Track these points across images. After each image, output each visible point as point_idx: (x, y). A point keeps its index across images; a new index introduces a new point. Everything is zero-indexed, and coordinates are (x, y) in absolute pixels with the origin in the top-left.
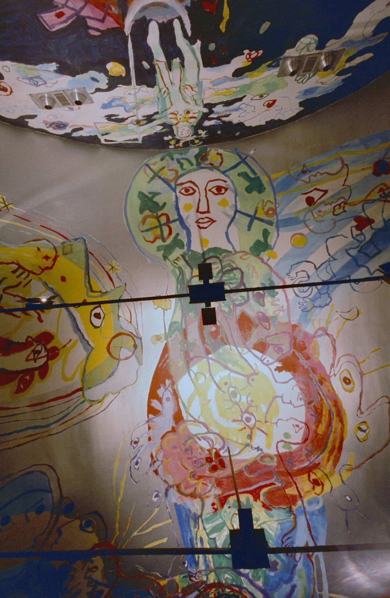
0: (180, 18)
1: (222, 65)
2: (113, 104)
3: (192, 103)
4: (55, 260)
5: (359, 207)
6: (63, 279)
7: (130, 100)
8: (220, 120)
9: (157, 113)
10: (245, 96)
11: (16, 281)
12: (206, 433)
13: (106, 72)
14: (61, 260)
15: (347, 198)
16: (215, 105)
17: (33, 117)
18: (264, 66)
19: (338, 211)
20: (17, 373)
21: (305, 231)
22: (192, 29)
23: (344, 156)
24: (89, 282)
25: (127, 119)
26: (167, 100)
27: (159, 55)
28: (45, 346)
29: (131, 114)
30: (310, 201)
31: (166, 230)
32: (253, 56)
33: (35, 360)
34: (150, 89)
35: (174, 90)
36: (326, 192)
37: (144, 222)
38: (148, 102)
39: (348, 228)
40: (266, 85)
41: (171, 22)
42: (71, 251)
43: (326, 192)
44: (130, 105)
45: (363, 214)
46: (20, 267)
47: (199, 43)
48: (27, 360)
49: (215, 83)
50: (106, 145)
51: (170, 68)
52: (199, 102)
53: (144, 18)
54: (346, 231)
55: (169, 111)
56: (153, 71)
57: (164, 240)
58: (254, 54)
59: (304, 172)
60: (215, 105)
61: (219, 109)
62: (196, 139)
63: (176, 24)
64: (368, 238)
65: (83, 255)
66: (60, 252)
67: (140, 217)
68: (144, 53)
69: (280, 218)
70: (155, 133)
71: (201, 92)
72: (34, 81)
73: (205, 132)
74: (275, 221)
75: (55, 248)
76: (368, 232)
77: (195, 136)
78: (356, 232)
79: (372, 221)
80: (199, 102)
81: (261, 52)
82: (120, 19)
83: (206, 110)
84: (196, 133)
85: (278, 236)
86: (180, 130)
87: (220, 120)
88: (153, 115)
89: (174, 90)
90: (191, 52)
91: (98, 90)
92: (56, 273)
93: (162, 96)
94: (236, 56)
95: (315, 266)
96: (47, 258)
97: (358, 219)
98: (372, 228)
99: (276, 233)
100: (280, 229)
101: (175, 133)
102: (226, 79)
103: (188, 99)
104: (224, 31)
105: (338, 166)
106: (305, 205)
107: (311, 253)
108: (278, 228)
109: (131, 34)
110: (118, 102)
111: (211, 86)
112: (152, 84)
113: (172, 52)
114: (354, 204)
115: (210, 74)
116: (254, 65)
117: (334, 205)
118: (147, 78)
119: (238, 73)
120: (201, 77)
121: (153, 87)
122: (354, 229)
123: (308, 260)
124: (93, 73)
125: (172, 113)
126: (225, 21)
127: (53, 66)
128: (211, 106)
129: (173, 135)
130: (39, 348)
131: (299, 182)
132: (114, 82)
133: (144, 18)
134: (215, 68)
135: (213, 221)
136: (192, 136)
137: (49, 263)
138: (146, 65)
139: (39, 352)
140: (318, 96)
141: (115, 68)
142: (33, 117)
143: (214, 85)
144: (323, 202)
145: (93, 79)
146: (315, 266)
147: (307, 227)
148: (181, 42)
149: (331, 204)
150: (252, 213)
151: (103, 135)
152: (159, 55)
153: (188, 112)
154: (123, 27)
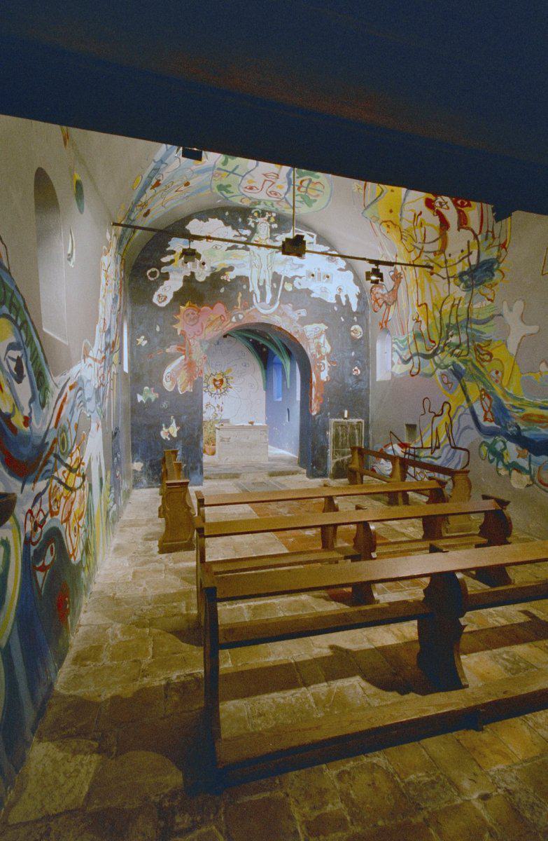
1: (300, 444)
4: (386, 222)
5: (158, 191)
6: (391, 211)
11: (409, 238)
13: (293, 286)
14: (383, 218)
17: (341, 270)
19: (170, 184)
20: (459, 212)
24: (380, 196)
27: (268, 288)
28: (434, 201)
30: (187, 184)
31: (305, 184)
33: (446, 203)
35: (264, 267)
36: (176, 191)
37: (318, 196)
42: (374, 216)
43: (176, 191)
46: (402, 238)
48: (448, 208)
49: (242, 265)
50: (315, 232)
51: (265, 281)
56: (273, 281)
57: (310, 181)
60: (243, 248)
63: (259, 301)
65: (369, 210)
66: (379, 222)
67: (318, 199)
68: (274, 291)
72: (325, 291)
75: (380, 225)
77: (257, 221)
78: (161, 178)
82: (279, 307)
84: (256, 224)
86: (265, 233)
89: (264, 267)
90: (254, 286)
91: (300, 277)
92: (391, 217)
96: (388, 226)
101: (269, 230)
104: (240, 293)
106: (191, 182)
110: (295, 267)
112: (275, 273)
113: (262, 288)
115: (244, 272)
118: (276, 278)
119: (231, 269)
124: (299, 287)
127: (313, 295)
129: (270, 227)
130: (438, 204)
135: (265, 175)
137: (390, 224)
139: (440, 203)
141: (289, 287)
142: (341, 270)
143: (243, 264)
145: (300, 284)
148: (258, 292)
151: (312, 243)
152: (268, 288)
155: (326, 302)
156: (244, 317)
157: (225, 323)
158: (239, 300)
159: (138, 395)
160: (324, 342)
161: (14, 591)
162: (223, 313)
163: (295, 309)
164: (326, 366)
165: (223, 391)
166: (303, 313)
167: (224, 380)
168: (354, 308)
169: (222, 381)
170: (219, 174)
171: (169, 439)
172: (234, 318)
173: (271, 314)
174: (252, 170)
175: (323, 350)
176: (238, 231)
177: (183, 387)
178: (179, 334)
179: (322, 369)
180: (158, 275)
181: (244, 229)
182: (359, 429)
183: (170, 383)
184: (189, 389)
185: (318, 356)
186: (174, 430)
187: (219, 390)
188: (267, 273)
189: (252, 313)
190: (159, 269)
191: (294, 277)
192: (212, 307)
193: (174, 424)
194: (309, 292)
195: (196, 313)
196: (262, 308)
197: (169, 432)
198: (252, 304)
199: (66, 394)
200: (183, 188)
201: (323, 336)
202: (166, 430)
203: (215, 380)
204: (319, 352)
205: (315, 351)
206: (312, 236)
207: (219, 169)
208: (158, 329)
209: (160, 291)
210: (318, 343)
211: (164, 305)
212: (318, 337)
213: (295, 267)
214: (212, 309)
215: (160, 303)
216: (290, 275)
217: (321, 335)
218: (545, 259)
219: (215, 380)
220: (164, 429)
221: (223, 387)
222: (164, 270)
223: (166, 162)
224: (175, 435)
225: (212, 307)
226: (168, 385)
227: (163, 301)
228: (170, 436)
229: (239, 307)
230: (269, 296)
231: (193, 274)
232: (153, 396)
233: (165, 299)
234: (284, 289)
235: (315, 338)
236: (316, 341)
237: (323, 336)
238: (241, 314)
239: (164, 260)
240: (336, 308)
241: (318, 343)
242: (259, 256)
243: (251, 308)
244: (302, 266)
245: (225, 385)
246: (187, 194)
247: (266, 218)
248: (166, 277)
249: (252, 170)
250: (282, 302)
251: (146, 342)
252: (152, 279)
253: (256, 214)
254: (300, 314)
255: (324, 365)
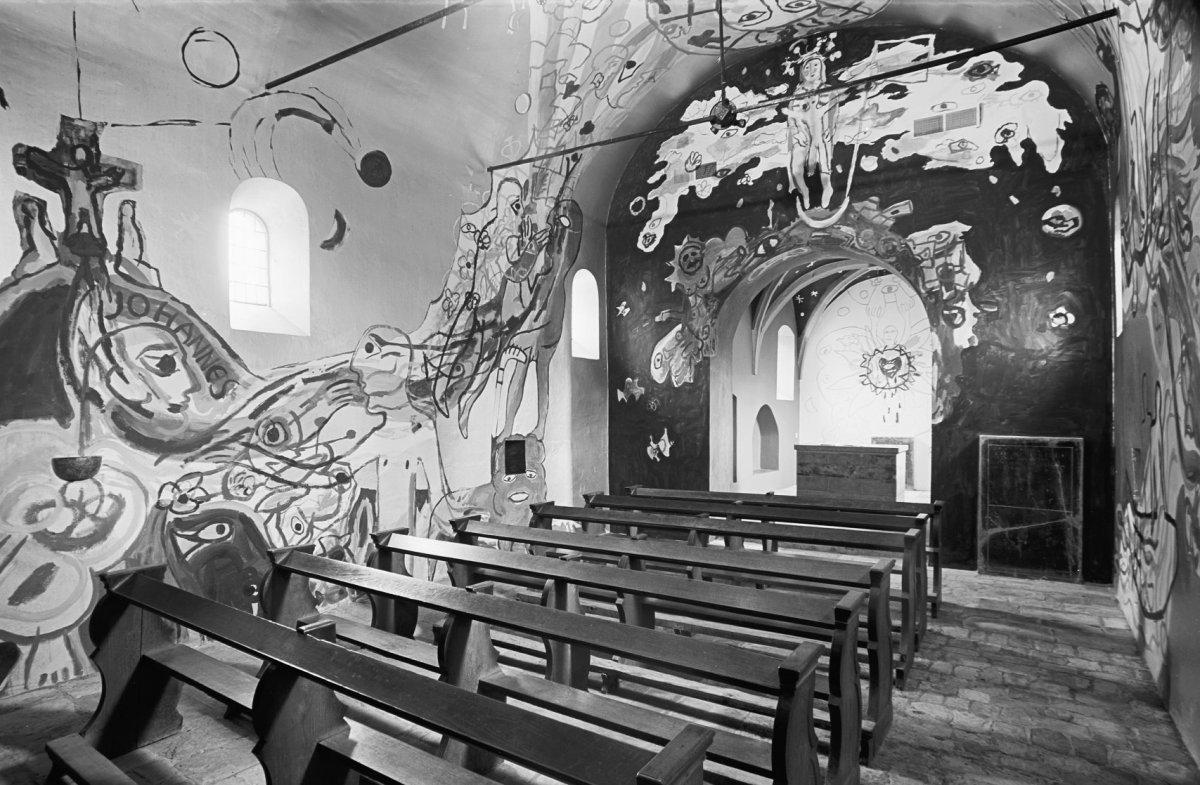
0: (804, 209)
2: (888, 117)
3: (800, 123)
5: (582, 96)
7: (867, 123)
8: (768, 96)
9: (842, 104)
10: (745, 134)
12: (448, 383)
15: (598, 92)
16: (776, 120)
17: (1008, 86)
18: (733, 170)
19: (599, 77)
21: (618, 41)
22: (795, 202)
23: (622, 110)
25: (881, 92)
26: (826, 127)
29: (872, 101)
30: (631, 64)
32: (744, 179)
34: (841, 141)
35: (818, 140)
36: (620, 81)
38: (848, 122)
39: (579, 75)
40: (726, 149)
41: (811, 207)
43: (620, 81)
44: (869, 117)
45: (575, 94)
47: (790, 191)
49: (776, 149)
52: (792, 123)
53: (831, 210)
54: (579, 73)
55: (827, 108)
58: (744, 181)
59: (651, 78)
60: (776, 120)
61: (771, 114)
62: (797, 57)
63: (807, 205)
64: (558, 85)
69: (656, 31)
70: (851, 65)
71: (790, 137)
73: (786, 72)
74: (660, 27)
76: (562, 89)
78: (571, 78)
79: (564, 98)
80: (792, 123)
81: (739, 183)
82: (850, 209)
83: (785, 111)
84: (797, 67)
85: (648, 17)
87: (768, 96)
88: (847, 100)
91: (896, 137)
93: (831, 131)
94: (759, 179)
95: (586, 22)
97: (576, 88)
98: (561, 94)
99: (652, 16)
100: (649, 24)
101: (824, 67)
102: (767, 154)
103: (803, 126)
105: (621, 103)
107: (598, 29)
108: (653, 22)
109: (845, 197)
110: (883, 120)
111: (780, 146)
114: (588, 93)
115: (780, 160)
116: (742, 169)
117: (605, 78)
118: (842, 152)
119: (754, 162)
120: (789, 156)
121: (838, 143)
122: (574, 79)
123: (596, 22)
125: (824, 104)
126: (770, 208)
128: (781, 118)
129: (827, 62)
131: (651, 68)
132: (874, 149)
133: (831, 210)
134: (776, 167)
136: (802, 63)
138: (839, 169)
140: (673, 137)
143: (776, 147)
144: (617, 73)
146: (586, 22)
147: (618, 46)
148: (805, 191)
149: (608, 78)
150: (693, 17)
153: (805, 107)
154: (850, 203)
155: (966, 171)
156: (779, 241)
157: (746, 260)
158: (770, 214)
159: (619, 391)
160: (962, 261)
161: (126, 538)
162: (743, 242)
163: (882, 206)
164: (969, 315)
165: (900, 381)
166: (905, 208)
167: (904, 359)
168: (1053, 165)
169: (898, 362)
170: (674, 27)
171: (658, 460)
172: (761, 247)
173: (832, 227)
174: (541, 44)
175: (959, 279)
176: (764, 93)
177: (683, 376)
178: (673, 290)
179: (958, 320)
180: (644, 204)
181: (775, 86)
182: (1065, 462)
183: (660, 371)
184: (688, 378)
185: (946, 295)
186: (665, 445)
187: (891, 381)
188: (822, 150)
189: (794, 233)
190: (646, 197)
191: (881, 143)
192: (723, 236)
193: (665, 436)
194: (919, 160)
195: (698, 251)
196: (814, 218)
197: (658, 448)
198: (796, 215)
199: (292, 387)
200: (628, 72)
201: (959, 247)
202: (654, 446)
203: (884, 361)
204: (950, 286)
205: (937, 283)
206: (925, 42)
207: (664, 21)
208: (644, 288)
209: (647, 230)
210: (946, 265)
211: (651, 249)
212: (947, 250)
213: (883, 120)
214: (724, 240)
215: (646, 247)
216: (870, 140)
217: (954, 243)
218: (349, 142)
219: (884, 361)
220: (652, 443)
221: (900, 373)
222: (651, 196)
223: (560, 57)
224: (667, 454)
225: (723, 236)
226: (658, 375)
227: (650, 244)
228: (661, 454)
229: (771, 226)
230: (828, 192)
231: (692, 189)
232: (639, 391)
233: (653, 241)
234: (859, 170)
235: (937, 256)
236: (939, 261)
237: (959, 247)
238: (773, 237)
239: (651, 180)
240: (993, 180)
241: (946, 265)
242: (805, 123)
243: (792, 224)
244: (900, 112)
245: (904, 369)
246: (646, 76)
247: (817, 49)
248: (654, 205)
249: (541, 44)
250: (854, 198)
251: (628, 310)
252: (635, 214)
253: (797, 50)
254: (897, 211)
255: (962, 311)
